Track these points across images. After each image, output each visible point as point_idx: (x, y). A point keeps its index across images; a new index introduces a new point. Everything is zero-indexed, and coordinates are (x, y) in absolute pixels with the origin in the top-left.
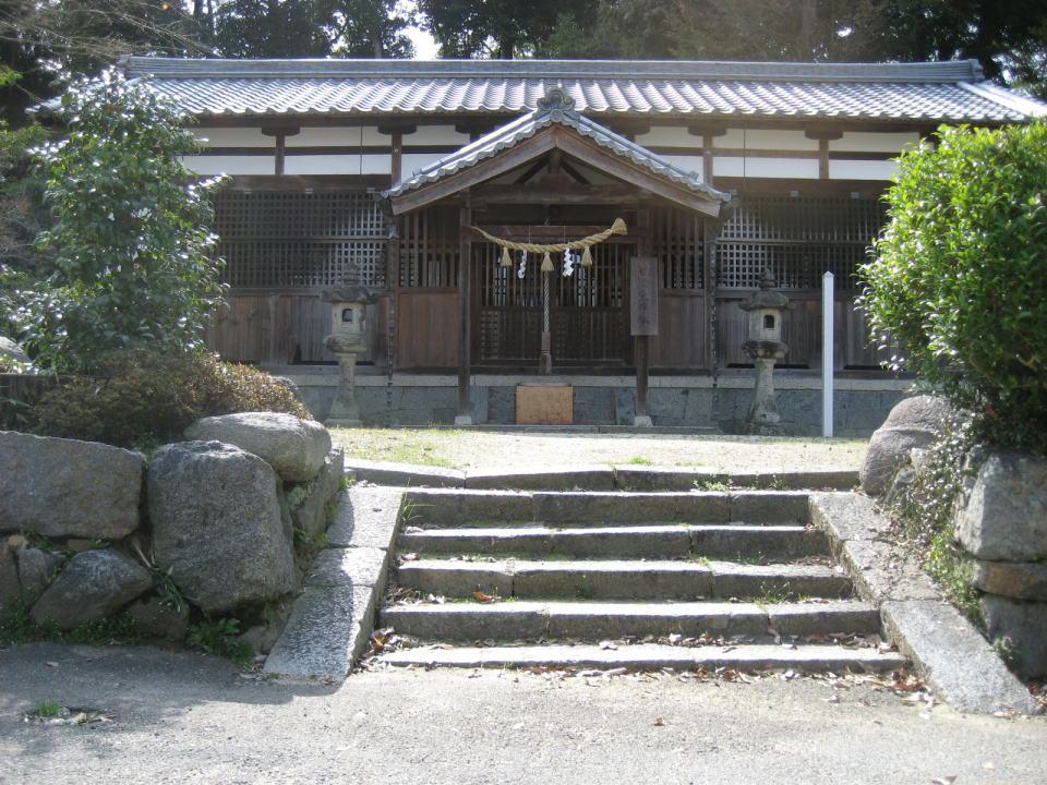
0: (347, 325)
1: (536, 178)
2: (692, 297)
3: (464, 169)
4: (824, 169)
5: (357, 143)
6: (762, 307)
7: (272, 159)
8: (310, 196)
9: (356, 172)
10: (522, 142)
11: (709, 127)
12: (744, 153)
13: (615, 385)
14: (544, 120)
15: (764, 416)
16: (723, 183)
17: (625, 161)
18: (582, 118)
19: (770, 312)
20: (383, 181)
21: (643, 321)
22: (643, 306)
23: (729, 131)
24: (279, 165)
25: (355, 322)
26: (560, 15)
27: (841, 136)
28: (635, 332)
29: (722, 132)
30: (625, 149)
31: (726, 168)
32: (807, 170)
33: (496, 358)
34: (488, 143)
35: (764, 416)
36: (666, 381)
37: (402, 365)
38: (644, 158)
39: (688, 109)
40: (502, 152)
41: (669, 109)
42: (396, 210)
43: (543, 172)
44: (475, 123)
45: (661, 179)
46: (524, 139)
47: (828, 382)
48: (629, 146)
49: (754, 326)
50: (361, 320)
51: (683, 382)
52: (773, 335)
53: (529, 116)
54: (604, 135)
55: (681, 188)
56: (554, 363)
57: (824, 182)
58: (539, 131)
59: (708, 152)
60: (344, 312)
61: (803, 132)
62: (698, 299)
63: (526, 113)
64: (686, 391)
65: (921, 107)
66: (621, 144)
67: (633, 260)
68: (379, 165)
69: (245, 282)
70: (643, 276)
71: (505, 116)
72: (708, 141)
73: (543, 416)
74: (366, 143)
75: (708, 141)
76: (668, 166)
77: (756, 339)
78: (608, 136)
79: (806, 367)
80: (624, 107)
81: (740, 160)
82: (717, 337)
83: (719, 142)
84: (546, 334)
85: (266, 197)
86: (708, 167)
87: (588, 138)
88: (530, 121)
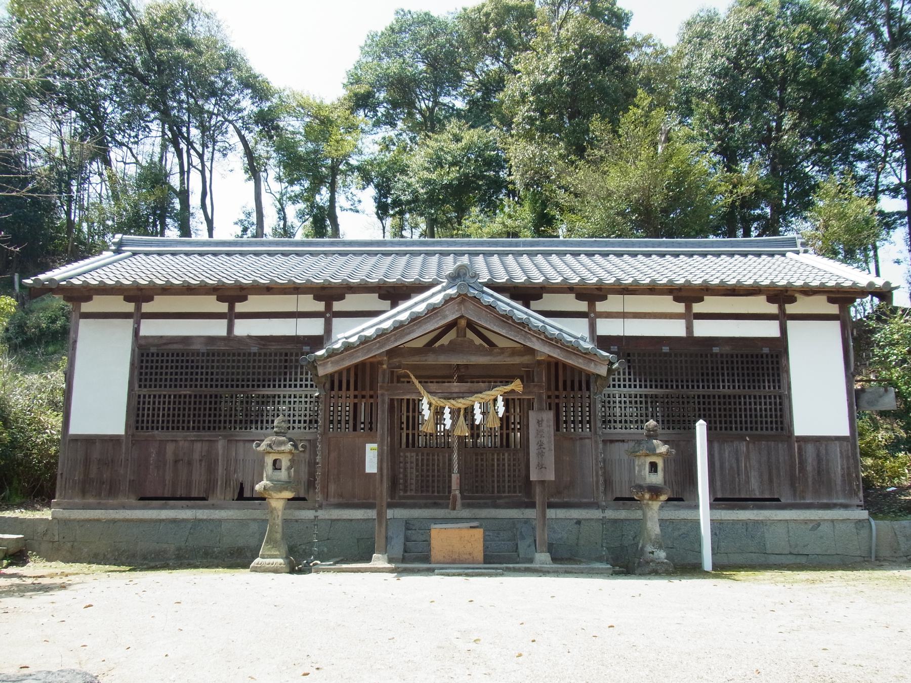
0: (277, 473)
1: (445, 341)
2: (581, 439)
3: (382, 335)
4: (689, 328)
5: (292, 309)
6: (647, 455)
7: (225, 322)
8: (255, 354)
9: (291, 333)
10: (433, 311)
11: (592, 293)
12: (624, 315)
13: (516, 516)
14: (452, 291)
15: (653, 553)
16: (604, 342)
17: (523, 326)
18: (485, 289)
19: (653, 459)
20: (316, 342)
21: (541, 467)
22: (541, 454)
23: (609, 296)
24: (230, 327)
25: (283, 470)
26: (475, 210)
27: (703, 300)
28: (533, 477)
29: (604, 298)
30: (525, 317)
31: (606, 328)
32: (676, 329)
33: (413, 493)
34: (403, 311)
35: (653, 553)
36: (561, 513)
37: (332, 500)
38: (541, 324)
39: (575, 280)
40: (416, 320)
41: (559, 279)
42: (321, 372)
43: (451, 335)
44: (394, 293)
45: (555, 342)
46: (434, 309)
47: (704, 514)
48: (526, 313)
49: (640, 471)
50: (289, 469)
51: (575, 514)
52: (657, 479)
53: (438, 288)
54: (505, 304)
55: (574, 350)
56: (463, 497)
57: (690, 340)
58: (448, 300)
59: (592, 315)
60: (275, 462)
61: (671, 297)
62: (587, 441)
63: (438, 284)
64: (579, 522)
65: (719, 274)
66: (519, 311)
67: (531, 413)
68: (313, 327)
69: (199, 428)
70: (540, 424)
71: (420, 288)
72: (592, 305)
73: (455, 556)
74: (301, 309)
75: (592, 305)
76: (561, 330)
77: (642, 483)
78: (508, 304)
79: (681, 500)
80: (520, 278)
81: (620, 321)
82: (604, 473)
83: (600, 306)
84: (455, 477)
85: (218, 355)
86: (593, 328)
87: (491, 307)
88: (440, 292)
